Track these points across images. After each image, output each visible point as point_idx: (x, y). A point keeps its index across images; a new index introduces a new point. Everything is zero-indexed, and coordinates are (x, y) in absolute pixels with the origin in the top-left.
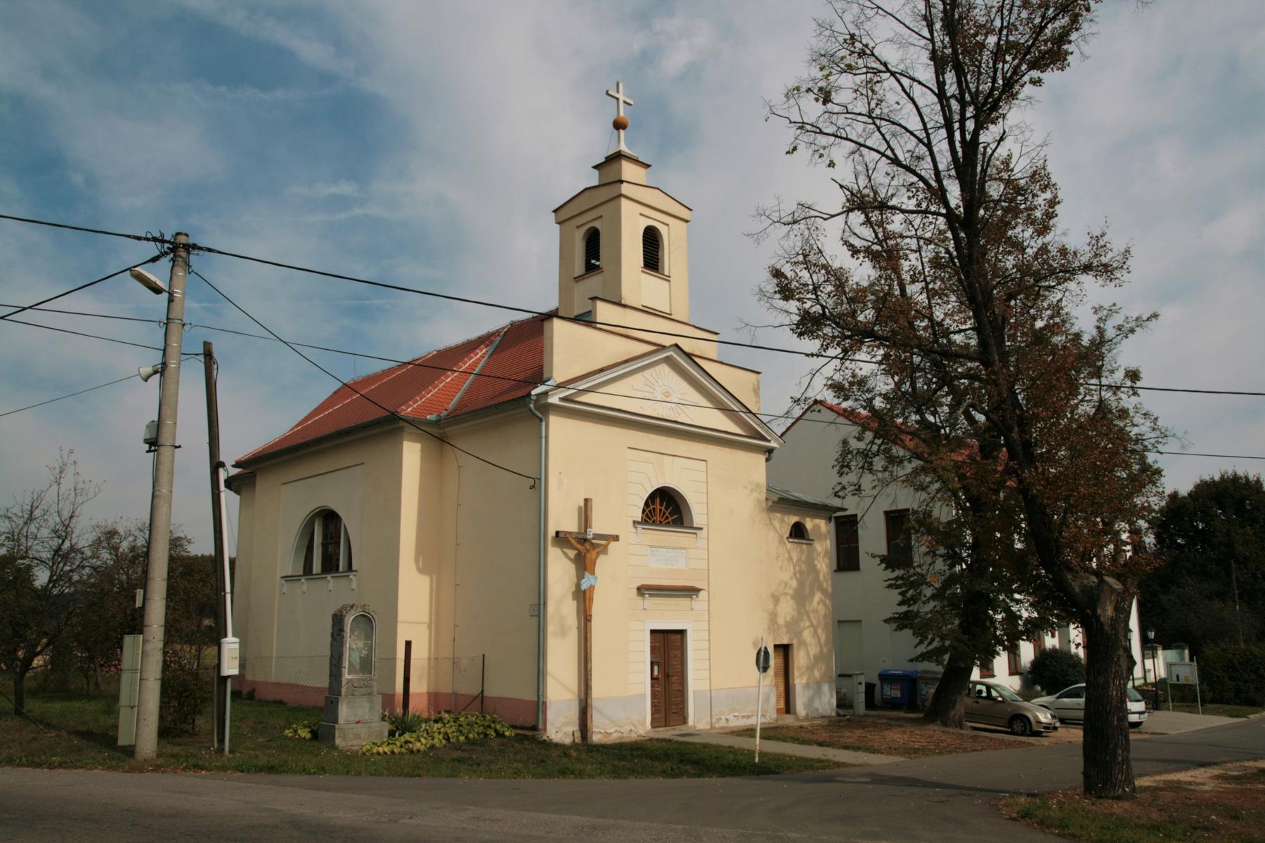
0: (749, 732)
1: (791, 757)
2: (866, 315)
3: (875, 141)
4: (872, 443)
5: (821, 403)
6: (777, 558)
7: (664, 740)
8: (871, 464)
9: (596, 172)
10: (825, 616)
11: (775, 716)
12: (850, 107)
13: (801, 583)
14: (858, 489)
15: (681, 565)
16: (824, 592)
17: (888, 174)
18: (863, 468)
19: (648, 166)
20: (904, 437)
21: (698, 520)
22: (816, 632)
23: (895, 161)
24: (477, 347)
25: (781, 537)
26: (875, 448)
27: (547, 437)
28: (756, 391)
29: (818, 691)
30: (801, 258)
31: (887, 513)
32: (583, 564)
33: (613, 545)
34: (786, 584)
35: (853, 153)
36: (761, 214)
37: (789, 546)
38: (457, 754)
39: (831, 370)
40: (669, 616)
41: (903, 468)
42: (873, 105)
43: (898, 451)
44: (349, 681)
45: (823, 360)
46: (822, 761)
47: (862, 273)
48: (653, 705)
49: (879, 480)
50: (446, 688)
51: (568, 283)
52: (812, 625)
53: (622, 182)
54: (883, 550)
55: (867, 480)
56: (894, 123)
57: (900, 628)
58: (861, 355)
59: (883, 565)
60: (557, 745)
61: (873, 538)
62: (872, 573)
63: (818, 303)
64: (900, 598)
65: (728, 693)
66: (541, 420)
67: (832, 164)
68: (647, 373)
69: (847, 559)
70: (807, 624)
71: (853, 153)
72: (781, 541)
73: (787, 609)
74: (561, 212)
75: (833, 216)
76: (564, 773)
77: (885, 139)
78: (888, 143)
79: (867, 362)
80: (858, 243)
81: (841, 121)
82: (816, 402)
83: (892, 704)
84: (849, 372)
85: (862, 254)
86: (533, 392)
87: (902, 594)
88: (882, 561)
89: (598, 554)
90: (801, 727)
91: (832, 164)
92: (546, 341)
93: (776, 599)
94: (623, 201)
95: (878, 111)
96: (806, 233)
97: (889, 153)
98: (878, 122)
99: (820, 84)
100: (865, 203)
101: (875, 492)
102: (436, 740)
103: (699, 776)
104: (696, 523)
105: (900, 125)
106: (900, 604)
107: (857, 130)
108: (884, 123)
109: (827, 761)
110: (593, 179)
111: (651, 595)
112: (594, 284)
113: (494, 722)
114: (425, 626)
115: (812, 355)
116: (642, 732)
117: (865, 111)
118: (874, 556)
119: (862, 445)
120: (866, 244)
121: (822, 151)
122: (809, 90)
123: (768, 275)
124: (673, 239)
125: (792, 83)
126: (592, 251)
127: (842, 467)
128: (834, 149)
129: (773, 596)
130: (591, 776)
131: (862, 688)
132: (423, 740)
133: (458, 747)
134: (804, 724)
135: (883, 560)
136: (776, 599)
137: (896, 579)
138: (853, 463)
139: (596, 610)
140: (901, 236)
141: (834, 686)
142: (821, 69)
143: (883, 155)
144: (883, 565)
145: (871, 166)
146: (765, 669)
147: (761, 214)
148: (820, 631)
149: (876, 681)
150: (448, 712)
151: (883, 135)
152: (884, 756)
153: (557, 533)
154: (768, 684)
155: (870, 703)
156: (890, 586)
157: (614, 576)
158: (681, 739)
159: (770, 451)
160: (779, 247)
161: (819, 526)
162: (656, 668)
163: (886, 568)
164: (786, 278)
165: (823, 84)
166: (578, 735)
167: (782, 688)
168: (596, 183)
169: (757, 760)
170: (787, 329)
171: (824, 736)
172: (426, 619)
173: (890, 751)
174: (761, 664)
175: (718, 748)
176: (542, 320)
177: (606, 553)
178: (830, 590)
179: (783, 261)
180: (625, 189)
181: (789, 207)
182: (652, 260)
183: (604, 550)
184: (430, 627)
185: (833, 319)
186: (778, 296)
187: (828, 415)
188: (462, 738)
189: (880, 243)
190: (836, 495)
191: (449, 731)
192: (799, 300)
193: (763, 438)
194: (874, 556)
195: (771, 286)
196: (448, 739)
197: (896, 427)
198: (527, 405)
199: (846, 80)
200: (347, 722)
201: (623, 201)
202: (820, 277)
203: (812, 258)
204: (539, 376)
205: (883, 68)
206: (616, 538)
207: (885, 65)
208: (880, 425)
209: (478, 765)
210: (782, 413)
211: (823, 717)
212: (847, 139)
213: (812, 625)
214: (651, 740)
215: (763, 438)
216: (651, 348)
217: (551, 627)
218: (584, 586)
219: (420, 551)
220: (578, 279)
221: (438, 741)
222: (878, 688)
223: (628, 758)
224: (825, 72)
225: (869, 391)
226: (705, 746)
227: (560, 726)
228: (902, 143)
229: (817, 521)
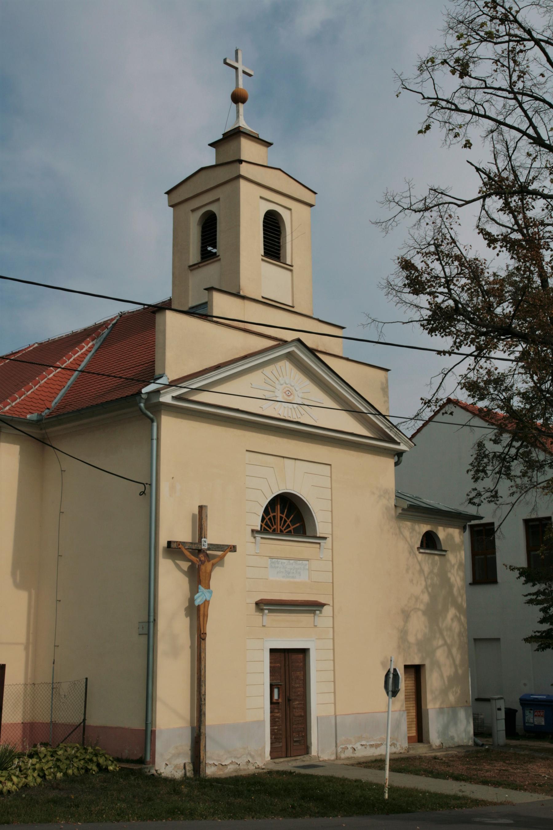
0: (377, 763)
1: (424, 793)
2: (505, 308)
3: (516, 118)
4: (510, 445)
5: (456, 403)
6: (407, 571)
7: (284, 773)
8: (509, 468)
9: (213, 150)
10: (460, 634)
11: (405, 745)
12: (489, 81)
13: (433, 597)
14: (495, 496)
15: (303, 578)
16: (458, 607)
17: (529, 155)
18: (499, 472)
19: (268, 144)
20: (543, 440)
21: (321, 529)
22: (450, 653)
23: (538, 141)
24: (83, 340)
25: (412, 547)
26: (513, 451)
27: (158, 439)
28: (385, 390)
29: (454, 718)
30: (432, 249)
31: (527, 522)
32: (197, 577)
33: (230, 556)
34: (417, 599)
35: (492, 131)
36: (391, 200)
37: (420, 556)
38: (53, 794)
39: (464, 366)
40: (289, 633)
41: (544, 473)
42: (515, 78)
43: (539, 455)
45: (456, 358)
46: (459, 798)
47: (499, 263)
48: (273, 733)
49: (517, 486)
50: (44, 717)
51: (182, 271)
52: (446, 643)
53: (241, 161)
54: (522, 562)
55: (504, 487)
56: (537, 99)
57: (542, 648)
58: (496, 354)
59: (523, 579)
60: (166, 780)
61: (511, 549)
62: (511, 586)
63: (451, 297)
64: (541, 615)
65: (354, 719)
66: (152, 421)
67: (468, 145)
68: (267, 370)
69: (483, 570)
70: (441, 642)
71: (492, 131)
72: (411, 551)
73: (418, 625)
74: (174, 194)
75: (468, 202)
76: (173, 813)
77: (527, 115)
78: (530, 120)
79: (503, 360)
80: (495, 230)
81: (479, 96)
82: (449, 401)
83: (535, 733)
84: (483, 372)
85: (499, 243)
86: (144, 391)
87: (544, 610)
88: (521, 574)
89: (213, 565)
90: (435, 758)
91: (468, 145)
92: (158, 336)
93: (406, 615)
94: (242, 182)
95: (520, 85)
96: (439, 221)
97: (531, 131)
98: (519, 97)
99: (456, 56)
100: (503, 187)
101: (513, 499)
102: (30, 778)
103: (323, 815)
104: (320, 532)
105: (544, 101)
106: (542, 622)
107: (496, 106)
108: (526, 98)
109: (464, 798)
110: (209, 158)
111: (270, 611)
112: (210, 273)
113: (96, 755)
114: (22, 648)
115: (444, 353)
116: (260, 764)
117: (505, 85)
118: (512, 569)
119: (498, 448)
120: (504, 230)
121: (457, 130)
122: (444, 62)
123: (395, 267)
124: (294, 220)
125: (426, 54)
126: (208, 238)
127: (477, 471)
128: (470, 128)
129: (403, 611)
130: (203, 816)
131: (502, 715)
132: (15, 779)
133: (55, 785)
134: (438, 754)
135: (523, 572)
136: (406, 615)
137: (537, 593)
138: (489, 468)
139: (211, 628)
140: (542, 223)
141: (470, 712)
142: (459, 38)
143: (524, 133)
144: (523, 579)
145: (512, 145)
146: (395, 693)
147: (391, 200)
148: (454, 651)
149: (517, 706)
150: (45, 745)
151: (525, 111)
152: (527, 794)
153: (169, 543)
154: (399, 708)
155: (511, 731)
156: (530, 602)
157: (231, 589)
158: (303, 771)
159: (399, 454)
160: (409, 236)
161: (452, 536)
162: (276, 691)
163: (526, 582)
164: (416, 269)
165: (460, 54)
166: (189, 767)
167: (413, 713)
168: (214, 163)
169: (386, 796)
170: (418, 325)
171: (460, 768)
173: (535, 787)
174: (390, 688)
175: (343, 781)
176: (154, 313)
177: (222, 565)
178: (465, 605)
179: (413, 252)
180: (244, 169)
181: (420, 192)
182: (273, 248)
183: (220, 561)
184: (27, 648)
185: (464, 313)
186: (407, 290)
187: (461, 416)
188: (59, 775)
189: (520, 230)
190: (471, 501)
191: (45, 767)
192: (430, 294)
193: (392, 441)
194: (512, 569)
195: (400, 279)
196: (43, 777)
197: (537, 429)
198: (137, 404)
199: (487, 50)
201: (242, 182)
202: (453, 269)
203: (445, 248)
204: (150, 374)
205: (527, 36)
206: (233, 549)
207: (529, 32)
208: (519, 426)
209: (77, 806)
210: (412, 417)
211: (459, 746)
212: (485, 116)
213: (446, 643)
214: (270, 772)
215: (392, 441)
216: (272, 343)
217: (162, 646)
218: (198, 601)
220: (193, 267)
221: (33, 779)
222: (519, 715)
223: (245, 791)
224: (463, 41)
225: (507, 389)
226: (330, 779)
227: (170, 759)
228: (546, 120)
229: (451, 530)
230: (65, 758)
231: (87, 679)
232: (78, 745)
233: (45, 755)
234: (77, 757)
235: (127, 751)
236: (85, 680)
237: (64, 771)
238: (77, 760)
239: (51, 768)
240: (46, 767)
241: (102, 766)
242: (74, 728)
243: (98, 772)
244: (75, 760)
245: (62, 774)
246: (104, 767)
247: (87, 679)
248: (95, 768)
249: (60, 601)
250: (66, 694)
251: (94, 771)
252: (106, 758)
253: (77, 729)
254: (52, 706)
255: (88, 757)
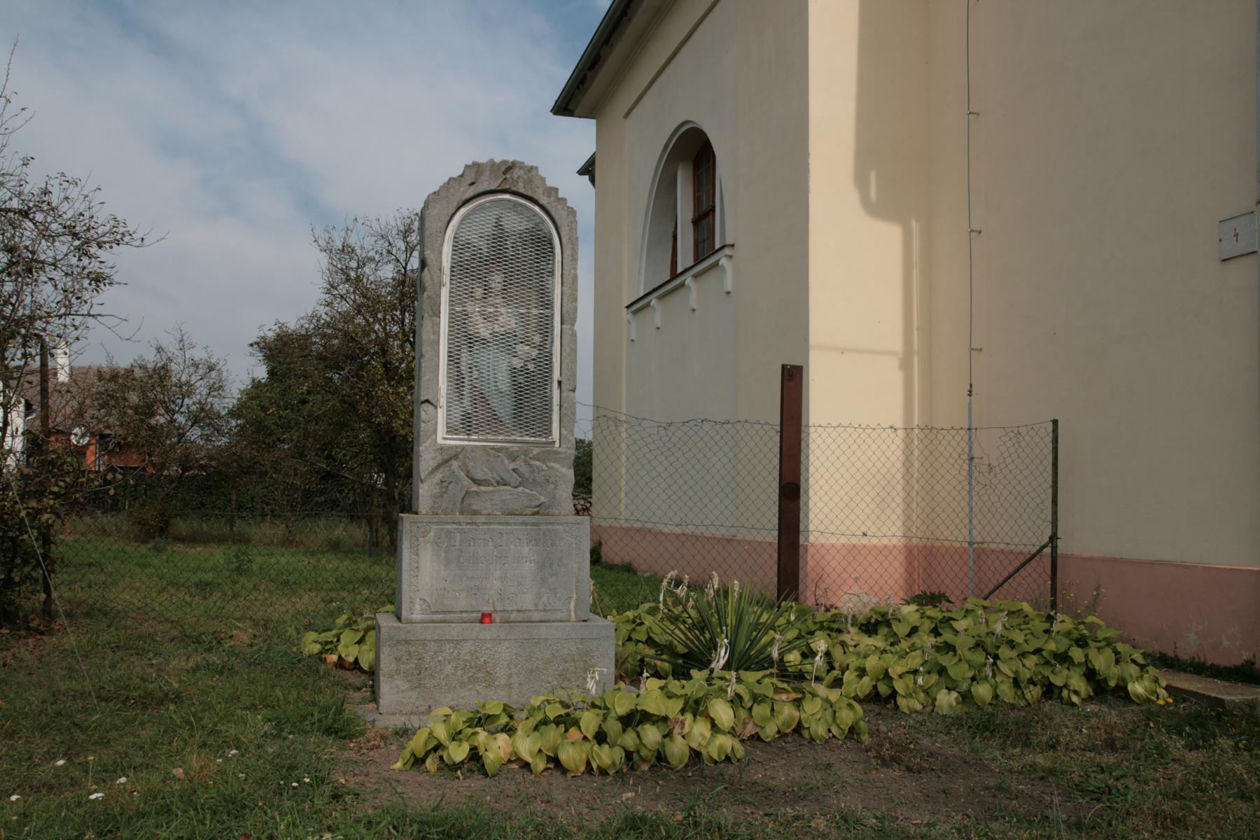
44: (449, 457)
50: (953, 534)
102: (812, 707)
113: (1081, 642)
172: (897, 344)
184: (906, 365)
188: (946, 700)
191: (896, 669)
200: (441, 615)
219: (870, 154)
230: (972, 642)
231: (1055, 422)
232: (1026, 607)
233: (914, 630)
234: (1012, 644)
235: (1192, 637)
236: (1050, 427)
237: (964, 687)
238: (1014, 654)
239: (915, 672)
240: (900, 669)
241: (1105, 680)
242: (1022, 560)
243: (1089, 699)
244: (1005, 652)
245: (954, 694)
246: (1112, 684)
247: (1055, 422)
248: (1078, 683)
249: (980, 232)
250: (994, 463)
251: (1076, 693)
252: (1116, 653)
253: (1033, 562)
254: (969, 504)
255: (1052, 646)
